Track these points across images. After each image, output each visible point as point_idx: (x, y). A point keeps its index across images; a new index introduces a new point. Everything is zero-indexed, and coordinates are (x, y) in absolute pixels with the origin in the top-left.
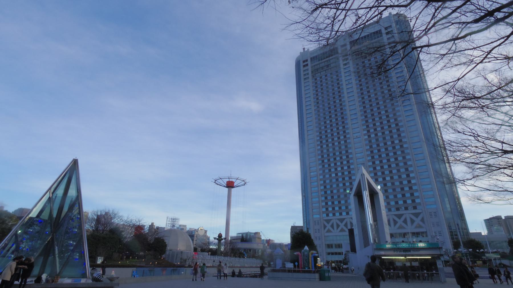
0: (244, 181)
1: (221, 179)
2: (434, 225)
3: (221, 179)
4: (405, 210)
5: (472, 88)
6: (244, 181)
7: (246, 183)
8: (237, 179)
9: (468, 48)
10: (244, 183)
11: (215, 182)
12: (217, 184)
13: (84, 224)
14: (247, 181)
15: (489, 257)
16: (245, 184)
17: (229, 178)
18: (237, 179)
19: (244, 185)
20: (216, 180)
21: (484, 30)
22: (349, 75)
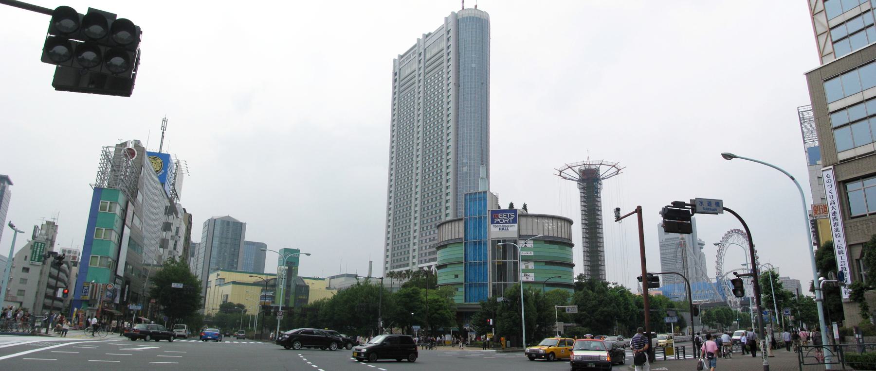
0: (614, 166)
1: (569, 167)
2: (553, 252)
3: (569, 167)
4: (692, 232)
5: (354, 298)
6: (614, 166)
7: (619, 170)
8: (601, 164)
9: (871, 159)
10: (616, 170)
11: (560, 175)
12: (565, 178)
13: (204, 244)
14: (620, 166)
15: (500, 352)
16: (618, 171)
17: (584, 164)
18: (601, 164)
19: (617, 174)
20: (561, 172)
21: (554, 244)
22: (281, 349)
